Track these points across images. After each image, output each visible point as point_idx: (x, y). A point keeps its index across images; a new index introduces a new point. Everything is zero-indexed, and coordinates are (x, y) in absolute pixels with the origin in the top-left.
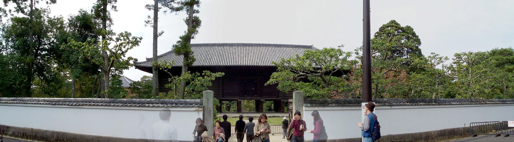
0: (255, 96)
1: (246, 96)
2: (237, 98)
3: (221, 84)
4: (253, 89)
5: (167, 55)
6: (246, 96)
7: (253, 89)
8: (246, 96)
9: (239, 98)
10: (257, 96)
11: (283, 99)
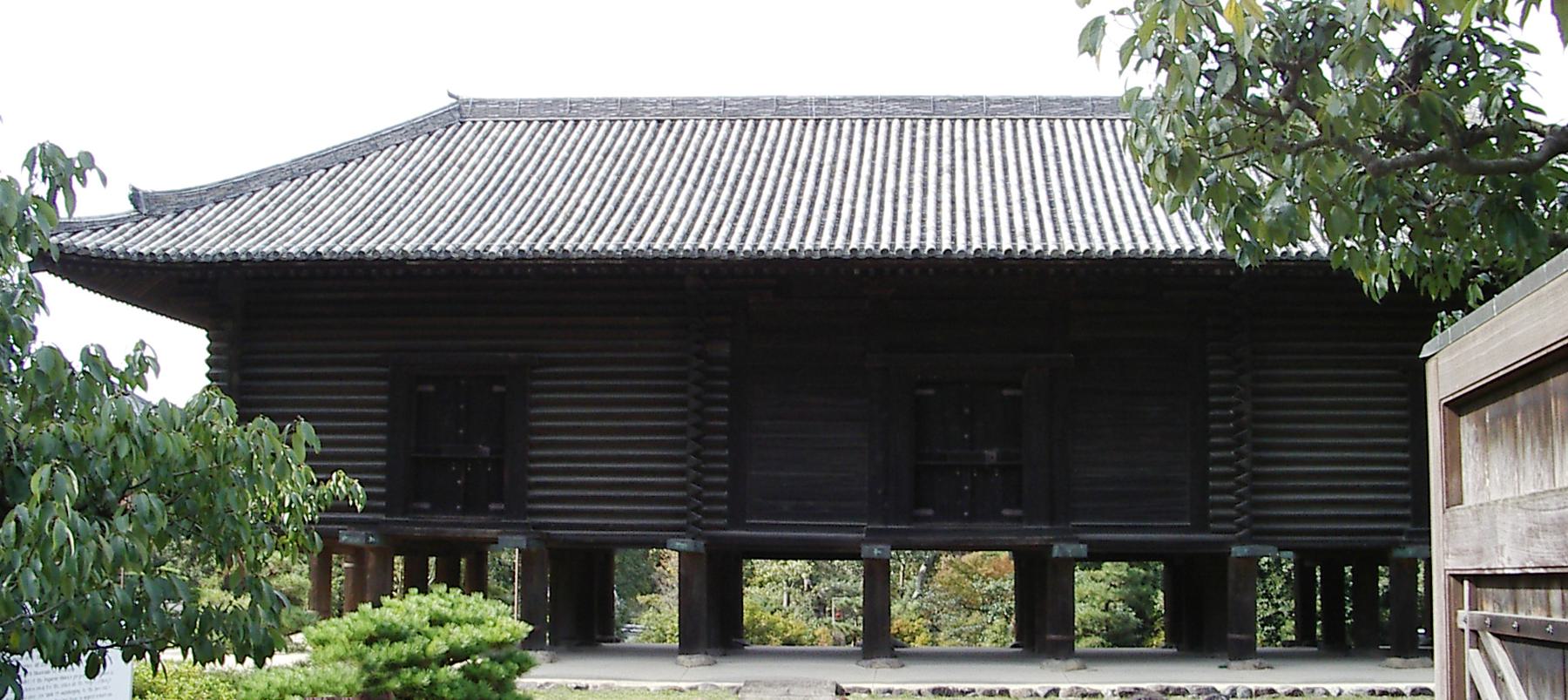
0: (1006, 512)
1: (424, 511)
2: (858, 529)
3: (720, 417)
4: (991, 454)
5: (555, 130)
6: (930, 512)
7: (991, 454)
8: (927, 519)
9: (869, 532)
10: (1019, 519)
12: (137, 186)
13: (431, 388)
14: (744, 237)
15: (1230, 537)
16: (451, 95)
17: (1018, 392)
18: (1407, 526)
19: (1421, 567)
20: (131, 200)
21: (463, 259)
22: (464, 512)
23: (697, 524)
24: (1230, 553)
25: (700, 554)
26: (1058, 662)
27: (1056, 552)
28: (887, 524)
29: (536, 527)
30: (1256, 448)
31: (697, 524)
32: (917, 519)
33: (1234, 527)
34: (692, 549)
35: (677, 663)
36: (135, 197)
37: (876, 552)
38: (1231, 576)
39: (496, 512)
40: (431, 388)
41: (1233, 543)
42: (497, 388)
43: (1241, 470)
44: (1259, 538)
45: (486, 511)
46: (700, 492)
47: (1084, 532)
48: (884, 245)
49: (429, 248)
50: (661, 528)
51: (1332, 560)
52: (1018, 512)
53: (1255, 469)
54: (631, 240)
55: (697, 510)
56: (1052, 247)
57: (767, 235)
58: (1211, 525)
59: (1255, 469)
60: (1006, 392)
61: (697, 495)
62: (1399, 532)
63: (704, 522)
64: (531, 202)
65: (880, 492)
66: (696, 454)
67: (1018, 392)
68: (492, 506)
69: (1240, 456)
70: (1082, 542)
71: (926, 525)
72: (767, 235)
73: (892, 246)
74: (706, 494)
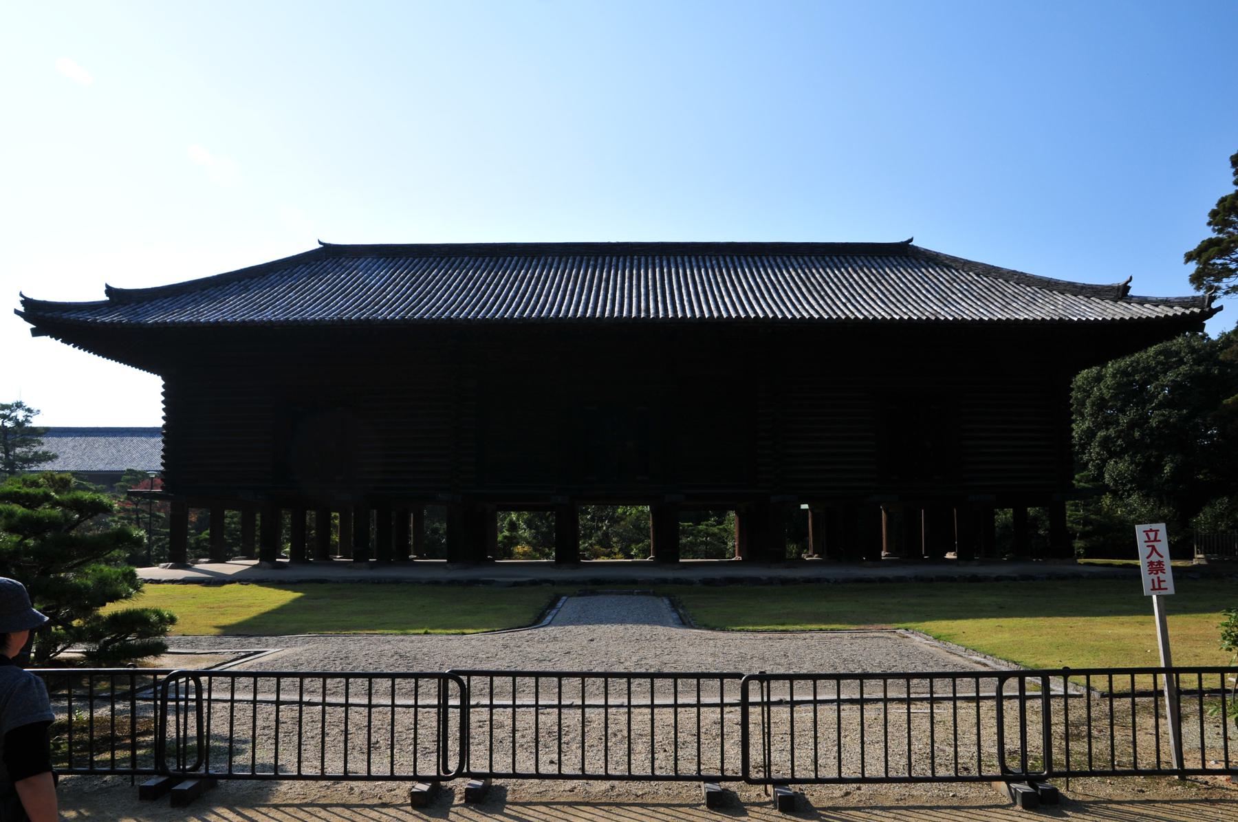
16: (320, 243)
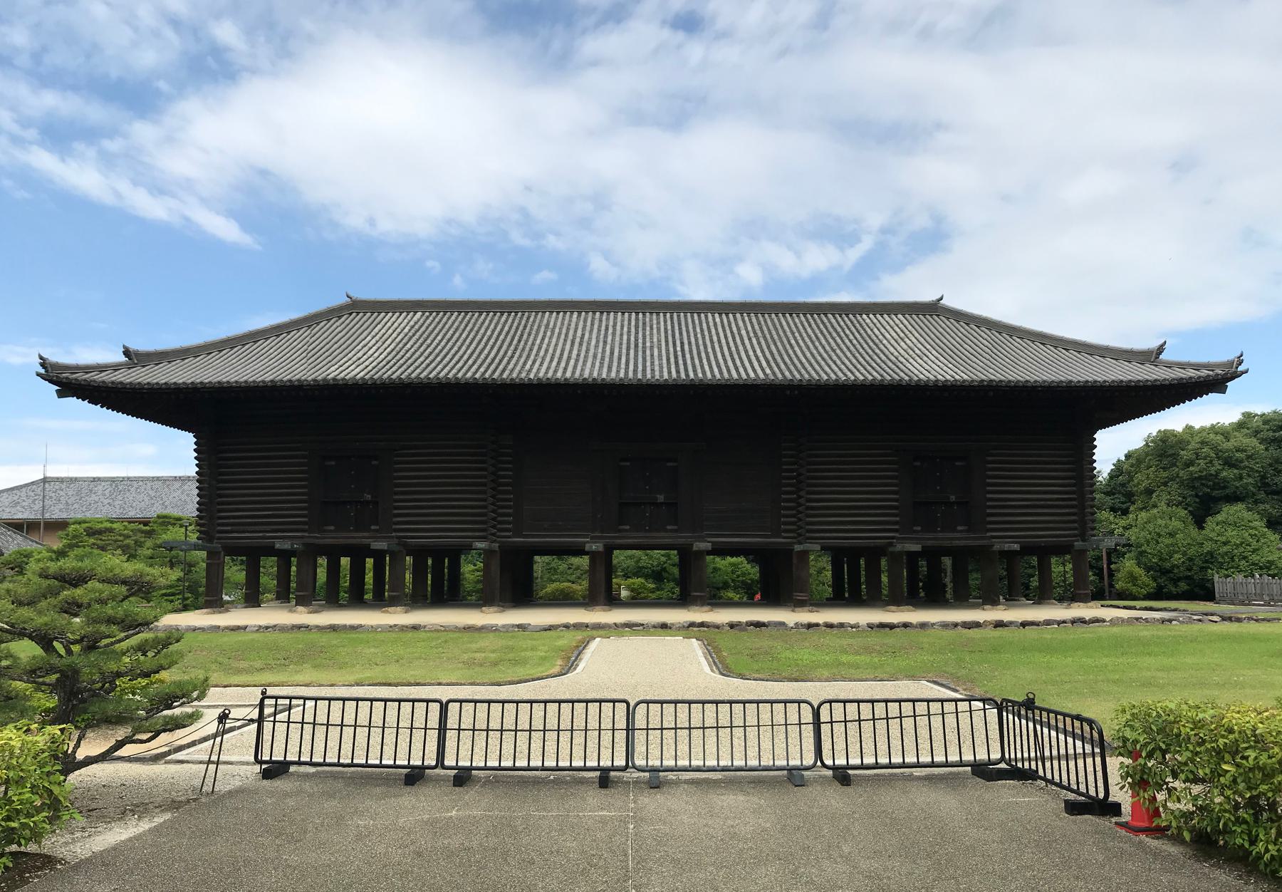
1: (626, 531)
10: (676, 531)
11: (800, 543)
12: (127, 345)
13: (333, 463)
14: (565, 369)
15: (794, 540)
17: (675, 464)
18: (897, 535)
19: (676, 527)
20: (124, 354)
21: (383, 383)
22: (356, 530)
23: (493, 534)
24: (793, 549)
25: (495, 551)
26: (697, 608)
27: (695, 548)
28: (603, 533)
29: (398, 537)
30: (809, 493)
31: (493, 534)
32: (620, 531)
33: (796, 535)
34: (487, 548)
35: (482, 612)
36: (127, 353)
37: (594, 547)
38: (795, 561)
39: (374, 530)
40: (333, 463)
41: (794, 543)
42: (374, 462)
43: (800, 505)
44: (810, 541)
45: (369, 530)
46: (496, 518)
47: (709, 537)
48: (622, 375)
49: (371, 378)
50: (469, 537)
51: (853, 554)
52: (676, 527)
53: (808, 504)
54: (489, 372)
55: (494, 527)
56: (709, 376)
57: (614, 369)
58: (783, 534)
59: (808, 504)
60: (669, 464)
61: (494, 519)
62: (893, 538)
63: (498, 534)
64: (1033, 356)
65: (599, 516)
66: (493, 497)
67: (675, 464)
68: (373, 527)
69: (800, 497)
70: (709, 542)
71: (624, 534)
72: (614, 369)
73: (653, 377)
74: (499, 519)
